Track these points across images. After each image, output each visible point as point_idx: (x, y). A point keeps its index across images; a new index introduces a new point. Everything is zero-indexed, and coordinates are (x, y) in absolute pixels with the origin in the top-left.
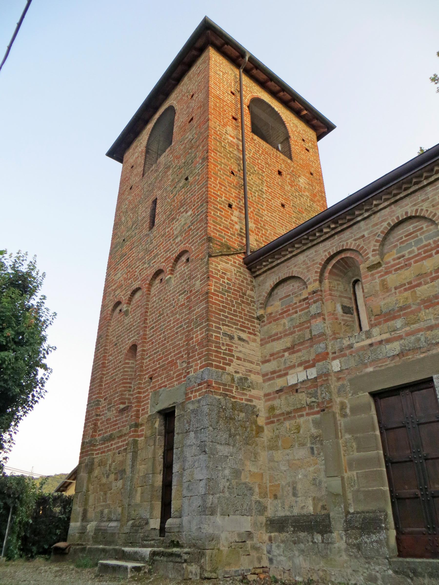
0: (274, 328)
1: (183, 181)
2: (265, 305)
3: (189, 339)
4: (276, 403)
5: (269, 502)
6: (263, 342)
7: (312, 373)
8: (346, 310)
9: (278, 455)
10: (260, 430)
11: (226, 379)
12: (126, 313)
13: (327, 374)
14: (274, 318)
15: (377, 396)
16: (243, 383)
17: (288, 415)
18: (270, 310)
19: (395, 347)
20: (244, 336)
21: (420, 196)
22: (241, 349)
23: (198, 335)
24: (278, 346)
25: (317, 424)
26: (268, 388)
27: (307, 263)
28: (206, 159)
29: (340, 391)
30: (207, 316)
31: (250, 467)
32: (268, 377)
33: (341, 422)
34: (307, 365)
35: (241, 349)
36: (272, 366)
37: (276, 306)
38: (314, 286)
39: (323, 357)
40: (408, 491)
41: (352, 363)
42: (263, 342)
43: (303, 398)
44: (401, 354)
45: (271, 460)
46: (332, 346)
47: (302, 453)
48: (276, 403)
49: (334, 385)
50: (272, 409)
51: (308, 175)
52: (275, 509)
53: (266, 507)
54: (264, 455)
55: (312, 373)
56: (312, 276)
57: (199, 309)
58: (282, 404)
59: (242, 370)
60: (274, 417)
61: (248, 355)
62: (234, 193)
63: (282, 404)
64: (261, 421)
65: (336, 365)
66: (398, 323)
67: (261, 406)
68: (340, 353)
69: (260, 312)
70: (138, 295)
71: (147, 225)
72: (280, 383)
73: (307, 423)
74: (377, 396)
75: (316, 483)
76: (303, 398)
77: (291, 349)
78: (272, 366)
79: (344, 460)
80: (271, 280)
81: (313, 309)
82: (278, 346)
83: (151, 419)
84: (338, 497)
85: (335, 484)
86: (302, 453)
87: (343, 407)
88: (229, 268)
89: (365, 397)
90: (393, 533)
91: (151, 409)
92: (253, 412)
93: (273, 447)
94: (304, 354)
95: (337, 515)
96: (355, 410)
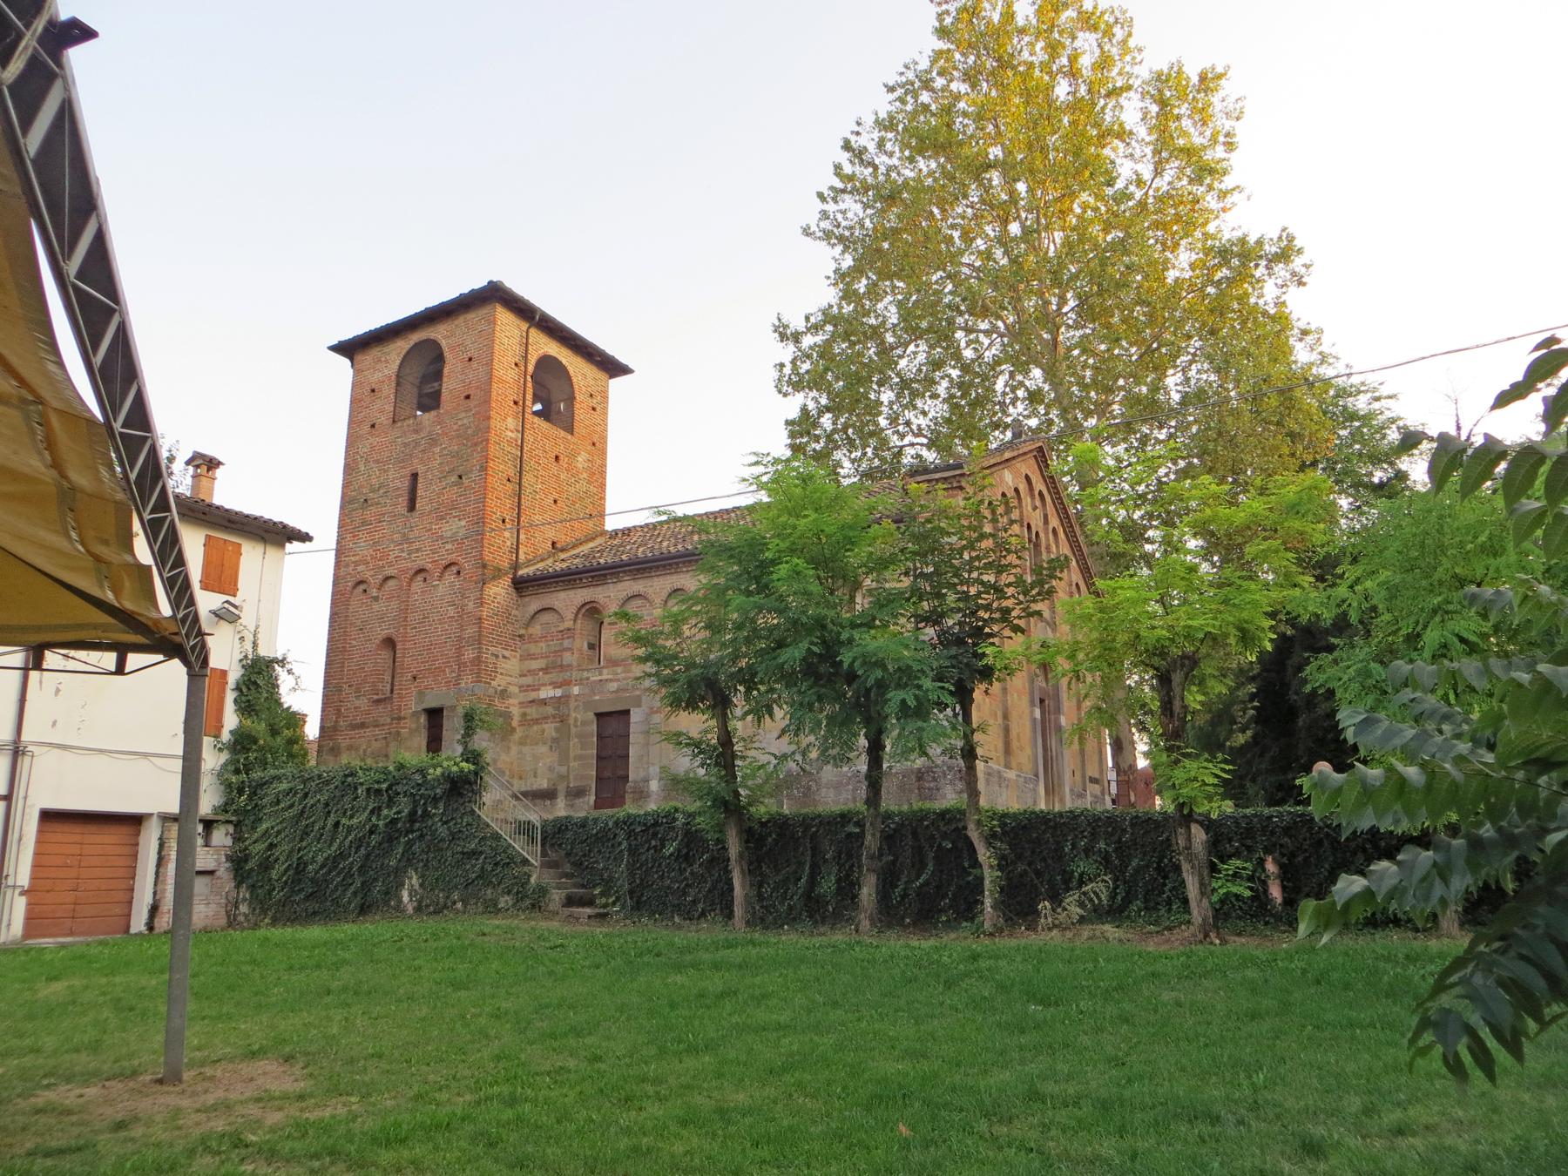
0: (533, 649)
1: (454, 478)
2: (527, 625)
3: (459, 655)
4: (528, 710)
5: (515, 782)
6: (523, 658)
7: (558, 692)
8: (591, 646)
9: (526, 749)
10: (513, 730)
11: (491, 691)
12: (376, 599)
13: (568, 696)
14: (533, 640)
15: (599, 716)
16: (504, 694)
17: (536, 721)
18: (531, 631)
19: (613, 686)
20: (507, 653)
21: (648, 582)
22: (504, 666)
23: (469, 654)
24: (535, 665)
25: (557, 730)
26: (523, 697)
27: (568, 600)
28: (484, 469)
29: (576, 707)
30: (479, 640)
31: (504, 757)
32: (525, 688)
33: (573, 730)
34: (556, 685)
35: (504, 666)
36: (528, 680)
37: (536, 630)
38: (569, 624)
39: (566, 683)
40: (607, 774)
41: (587, 691)
42: (523, 658)
43: (549, 710)
44: (617, 691)
45: (520, 752)
46: (575, 675)
47: (544, 749)
48: (528, 710)
49: (572, 704)
50: (524, 715)
51: (590, 448)
52: (519, 786)
53: (748, 923)
54: (514, 749)
55: (558, 692)
56: (569, 615)
57: (471, 631)
58: (533, 712)
59: (503, 683)
60: (525, 721)
61: (509, 670)
62: (508, 503)
63: (533, 712)
64: (515, 723)
65: (576, 690)
66: (619, 670)
67: (516, 712)
68: (580, 682)
69: (522, 632)
70: (391, 583)
71: (403, 501)
72: (533, 695)
73: (550, 729)
74: (599, 716)
75: (551, 769)
76: (549, 710)
77: (545, 670)
78: (528, 680)
79: (572, 755)
80: (534, 605)
81: (566, 643)
82: (535, 665)
83: (415, 714)
84: (562, 777)
85: (563, 770)
86: (544, 749)
87: (576, 720)
88: (499, 591)
89: (591, 716)
90: (593, 798)
91: (414, 706)
92: (507, 716)
93: (522, 743)
94: (555, 676)
95: (562, 788)
96: (584, 723)
